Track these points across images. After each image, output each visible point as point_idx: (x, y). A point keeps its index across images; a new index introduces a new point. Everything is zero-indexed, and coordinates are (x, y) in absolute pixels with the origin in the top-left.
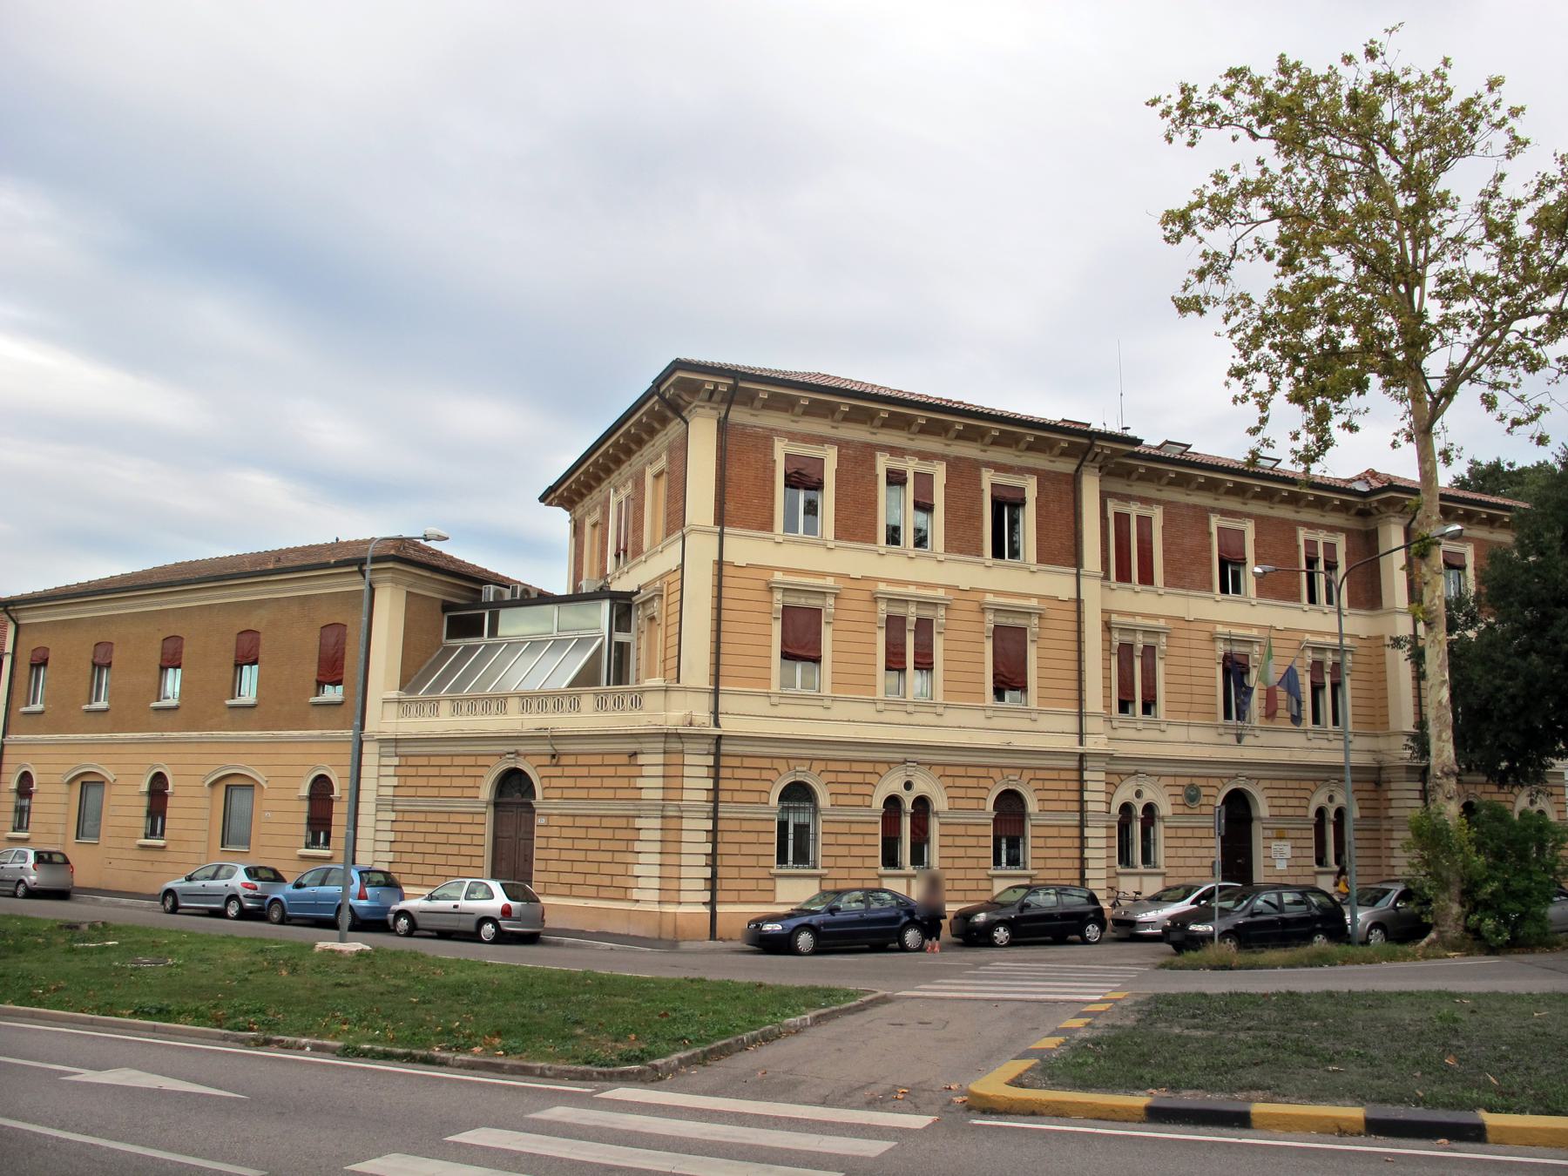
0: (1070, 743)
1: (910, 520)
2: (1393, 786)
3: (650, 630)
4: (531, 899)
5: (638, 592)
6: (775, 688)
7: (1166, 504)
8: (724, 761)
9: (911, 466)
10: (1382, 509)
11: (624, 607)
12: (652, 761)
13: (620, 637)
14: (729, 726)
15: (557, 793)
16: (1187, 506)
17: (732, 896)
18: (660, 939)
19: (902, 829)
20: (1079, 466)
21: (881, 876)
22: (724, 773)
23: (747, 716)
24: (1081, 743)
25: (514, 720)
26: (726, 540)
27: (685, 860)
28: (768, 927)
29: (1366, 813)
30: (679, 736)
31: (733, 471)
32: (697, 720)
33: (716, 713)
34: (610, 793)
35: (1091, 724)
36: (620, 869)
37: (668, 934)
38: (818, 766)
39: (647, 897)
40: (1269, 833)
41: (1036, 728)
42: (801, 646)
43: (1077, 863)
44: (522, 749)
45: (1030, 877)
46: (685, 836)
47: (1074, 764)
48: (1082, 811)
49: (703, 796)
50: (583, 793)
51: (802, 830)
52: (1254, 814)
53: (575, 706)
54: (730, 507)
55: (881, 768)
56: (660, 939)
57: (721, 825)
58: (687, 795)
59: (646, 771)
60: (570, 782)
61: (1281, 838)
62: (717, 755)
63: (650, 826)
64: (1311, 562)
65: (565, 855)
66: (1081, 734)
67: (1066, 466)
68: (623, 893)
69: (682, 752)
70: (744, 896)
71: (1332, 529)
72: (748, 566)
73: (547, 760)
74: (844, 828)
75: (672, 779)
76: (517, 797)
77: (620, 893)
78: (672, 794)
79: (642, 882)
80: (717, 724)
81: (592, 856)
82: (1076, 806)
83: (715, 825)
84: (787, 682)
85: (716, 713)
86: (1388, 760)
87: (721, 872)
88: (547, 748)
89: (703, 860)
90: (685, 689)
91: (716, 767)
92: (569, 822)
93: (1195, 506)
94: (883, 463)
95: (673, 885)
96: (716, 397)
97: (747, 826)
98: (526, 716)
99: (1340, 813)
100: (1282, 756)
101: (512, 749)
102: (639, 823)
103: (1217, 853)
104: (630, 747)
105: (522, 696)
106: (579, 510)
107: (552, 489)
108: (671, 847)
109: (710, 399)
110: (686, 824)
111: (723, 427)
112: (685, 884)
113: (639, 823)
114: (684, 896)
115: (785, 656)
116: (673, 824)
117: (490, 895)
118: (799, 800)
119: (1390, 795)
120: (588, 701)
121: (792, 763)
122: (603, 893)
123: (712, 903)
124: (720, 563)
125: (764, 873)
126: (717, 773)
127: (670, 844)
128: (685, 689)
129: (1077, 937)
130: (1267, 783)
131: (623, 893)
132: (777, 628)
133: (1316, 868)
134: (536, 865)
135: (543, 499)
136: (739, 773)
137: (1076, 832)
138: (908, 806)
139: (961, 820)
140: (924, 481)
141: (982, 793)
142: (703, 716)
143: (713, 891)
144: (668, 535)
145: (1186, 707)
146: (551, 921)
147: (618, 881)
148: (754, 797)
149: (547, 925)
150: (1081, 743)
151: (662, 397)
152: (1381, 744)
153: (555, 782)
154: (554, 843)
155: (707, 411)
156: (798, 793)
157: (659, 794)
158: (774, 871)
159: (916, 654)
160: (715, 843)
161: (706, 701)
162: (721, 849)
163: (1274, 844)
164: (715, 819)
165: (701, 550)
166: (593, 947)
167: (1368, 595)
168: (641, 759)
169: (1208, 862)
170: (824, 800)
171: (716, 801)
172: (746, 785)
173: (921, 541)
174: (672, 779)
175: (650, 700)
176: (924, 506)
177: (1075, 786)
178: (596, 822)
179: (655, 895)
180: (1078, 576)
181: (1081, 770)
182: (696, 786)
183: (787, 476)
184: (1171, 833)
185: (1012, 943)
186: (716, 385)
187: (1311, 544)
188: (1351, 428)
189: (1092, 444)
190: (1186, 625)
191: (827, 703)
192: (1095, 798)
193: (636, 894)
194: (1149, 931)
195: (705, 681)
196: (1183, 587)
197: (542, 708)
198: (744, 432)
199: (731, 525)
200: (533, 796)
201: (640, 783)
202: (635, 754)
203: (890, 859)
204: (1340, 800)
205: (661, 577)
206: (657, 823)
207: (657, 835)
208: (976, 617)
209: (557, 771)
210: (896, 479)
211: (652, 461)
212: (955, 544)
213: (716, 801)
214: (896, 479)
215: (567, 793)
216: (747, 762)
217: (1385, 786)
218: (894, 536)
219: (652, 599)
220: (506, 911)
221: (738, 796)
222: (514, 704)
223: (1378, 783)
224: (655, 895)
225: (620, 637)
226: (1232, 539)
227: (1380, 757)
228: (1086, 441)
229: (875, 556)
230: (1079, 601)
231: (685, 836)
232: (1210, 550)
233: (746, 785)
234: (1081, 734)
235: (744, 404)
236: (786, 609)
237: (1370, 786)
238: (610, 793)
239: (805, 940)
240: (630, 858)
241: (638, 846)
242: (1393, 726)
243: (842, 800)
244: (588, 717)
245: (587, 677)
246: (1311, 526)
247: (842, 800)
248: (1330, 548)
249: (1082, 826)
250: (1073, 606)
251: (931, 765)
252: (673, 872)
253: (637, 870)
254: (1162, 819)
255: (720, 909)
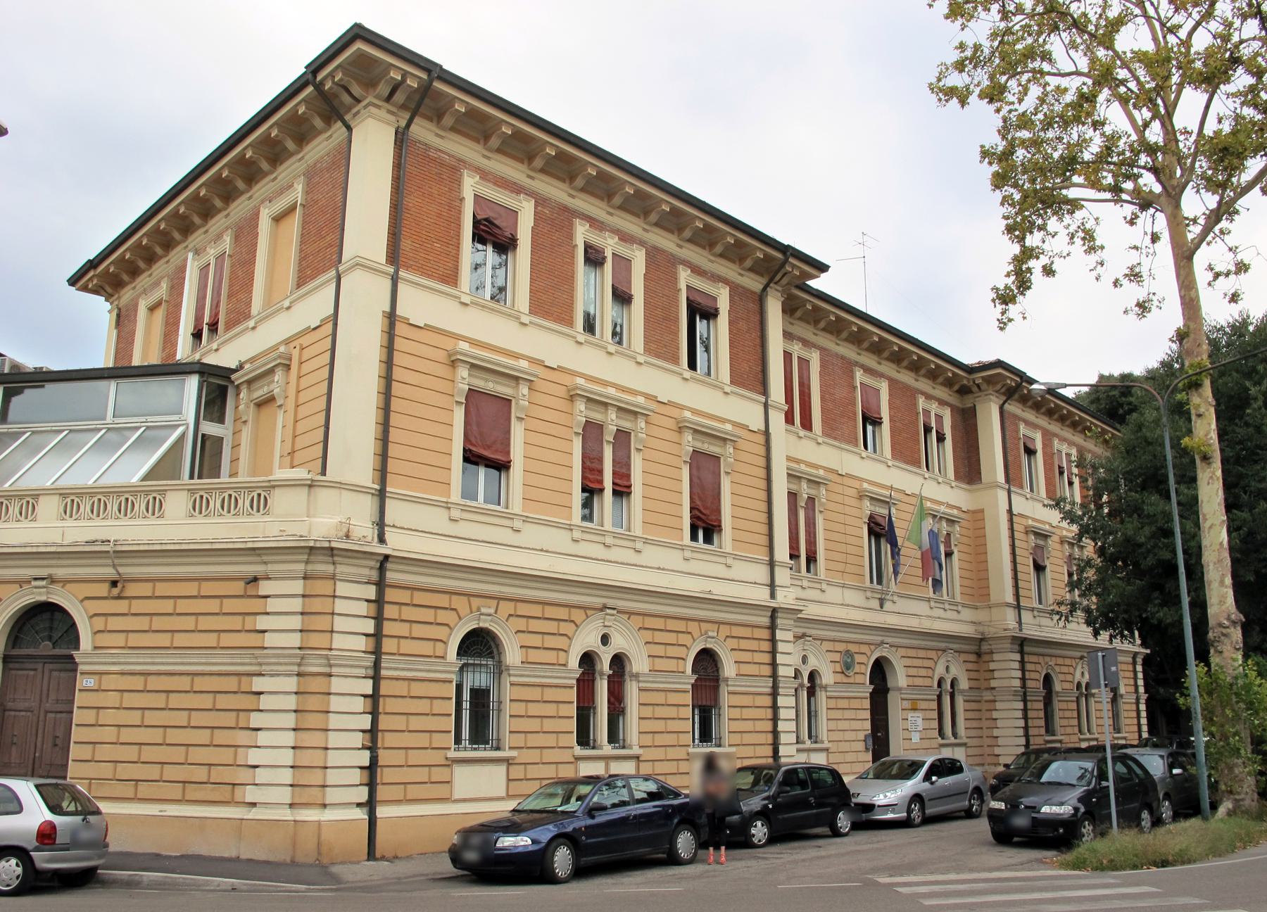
0: (760, 595)
1: (608, 313)
2: (996, 657)
3: (257, 420)
4: (88, 810)
5: (241, 367)
6: (456, 496)
7: (822, 350)
8: (390, 595)
9: (610, 245)
10: (984, 386)
11: (218, 388)
12: (284, 592)
13: (210, 428)
14: (397, 543)
15: (119, 640)
16: (837, 355)
17: (396, 792)
18: (293, 863)
19: (599, 690)
20: (765, 289)
21: (578, 759)
22: (389, 611)
23: (420, 531)
24: (773, 596)
25: (49, 528)
26: (402, 287)
27: (334, 740)
28: (507, 842)
29: (974, 684)
30: (331, 551)
31: (411, 201)
32: (357, 533)
33: (381, 524)
34: (211, 640)
35: (782, 576)
36: (225, 756)
37: (306, 852)
38: (506, 608)
39: (270, 798)
40: (906, 704)
41: (731, 575)
42: (486, 456)
43: (769, 738)
44: (60, 573)
45: (1125, 738)
46: (336, 703)
47: (766, 621)
48: (774, 676)
49: (361, 643)
50: (164, 640)
51: (480, 697)
52: (889, 685)
53: (156, 507)
54: (406, 245)
55: (577, 615)
56: (293, 863)
57: (385, 688)
58: (339, 642)
59: (272, 605)
60: (143, 623)
61: (914, 709)
62: (381, 584)
63: (279, 689)
64: (927, 430)
65: (127, 735)
66: (772, 586)
67: (754, 283)
68: (230, 793)
69: (333, 578)
70: (413, 791)
71: (942, 403)
72: (427, 328)
73: (103, 589)
74: (535, 694)
75: (315, 618)
76: (46, 648)
77: (224, 793)
78: (316, 640)
79: (261, 776)
80: (382, 540)
81: (174, 736)
82: (767, 670)
83: (376, 687)
84: (469, 493)
85: (381, 524)
86: (990, 632)
87: (384, 757)
88: (109, 572)
89: (358, 739)
90: (340, 486)
91: (379, 602)
92: (138, 683)
93: (843, 358)
94: (582, 233)
95: (315, 778)
96: (399, 97)
97: (417, 689)
98: (70, 523)
99: (953, 683)
100: (913, 624)
101: (43, 572)
102: (258, 684)
103: (868, 725)
104: (250, 568)
105: (63, 494)
106: (127, 295)
107: (92, 264)
108: (312, 720)
109: (388, 99)
110: (337, 685)
111: (401, 139)
112: (333, 777)
113: (258, 684)
114: (332, 796)
115: (466, 459)
116: (316, 684)
117: (14, 805)
118: (480, 655)
119: (992, 666)
120: (177, 503)
121: (476, 602)
122: (192, 793)
123: (370, 805)
124: (392, 317)
125: (437, 757)
126: (380, 611)
127: (310, 716)
128: (340, 486)
129: (825, 830)
130: (912, 653)
131: (230, 793)
132: (459, 416)
133: (940, 741)
134: (75, 751)
135: (73, 281)
136: (408, 613)
137: (767, 701)
138: (605, 665)
139: (660, 682)
140: (623, 264)
141: (679, 652)
142: (364, 529)
143: (372, 785)
144: (299, 286)
145: (840, 567)
146: (116, 844)
147: (218, 774)
148: (426, 648)
149: (112, 849)
150: (773, 596)
151: (319, 87)
152: (981, 616)
153: (114, 623)
154: (108, 717)
155: (382, 113)
156: (479, 644)
157: (295, 640)
158: (452, 754)
159: (614, 473)
160: (374, 713)
161: (367, 505)
162: (384, 723)
163: (910, 715)
164: (376, 678)
165: (365, 295)
166: (197, 887)
167: (969, 470)
168: (265, 588)
169: (861, 736)
170: (512, 655)
171: (377, 652)
172: (418, 630)
173: (617, 334)
174: (315, 618)
175: (280, 500)
176: (622, 298)
177: (766, 646)
178: (184, 683)
179: (285, 795)
180: (766, 406)
181: (773, 628)
182: (351, 630)
183: (476, 223)
184: (832, 703)
185: (773, 840)
186: (405, 75)
187: (927, 413)
188: (1048, 271)
189: (786, 261)
190: (839, 479)
191: (517, 524)
192: (789, 659)
193: (251, 794)
194: (890, 816)
195: (365, 475)
196: (835, 439)
197: (99, 509)
198: (429, 157)
199: (407, 268)
200: (76, 643)
201: (262, 623)
202: (255, 579)
203: (584, 737)
204: (954, 671)
205: (287, 342)
206: (291, 684)
207: (291, 702)
208: (673, 436)
209: (121, 606)
210: (594, 258)
211: (290, 184)
212: (653, 346)
213: (377, 652)
214: (594, 258)
215: (134, 640)
216: (420, 598)
217: (986, 658)
218: (590, 327)
219: (271, 371)
220: (47, 835)
221: (407, 646)
222: (49, 508)
223: (979, 655)
224: (285, 795)
225: (210, 428)
226: (870, 394)
227: (981, 629)
228: (779, 256)
229: (571, 343)
230: (767, 433)
231: (336, 703)
232: (854, 404)
233: (418, 630)
234: (772, 586)
235: (430, 119)
236: (472, 393)
237: (973, 658)
238: (211, 640)
239: (562, 859)
240: (242, 737)
241: (256, 720)
242: (994, 598)
243: (534, 656)
244: (177, 522)
245: (164, 469)
246: (929, 397)
247: (534, 656)
248: (939, 418)
249: (774, 694)
250: (761, 439)
251: (630, 614)
252: (314, 758)
253: (254, 757)
254: (636, 676)
255: (381, 812)
